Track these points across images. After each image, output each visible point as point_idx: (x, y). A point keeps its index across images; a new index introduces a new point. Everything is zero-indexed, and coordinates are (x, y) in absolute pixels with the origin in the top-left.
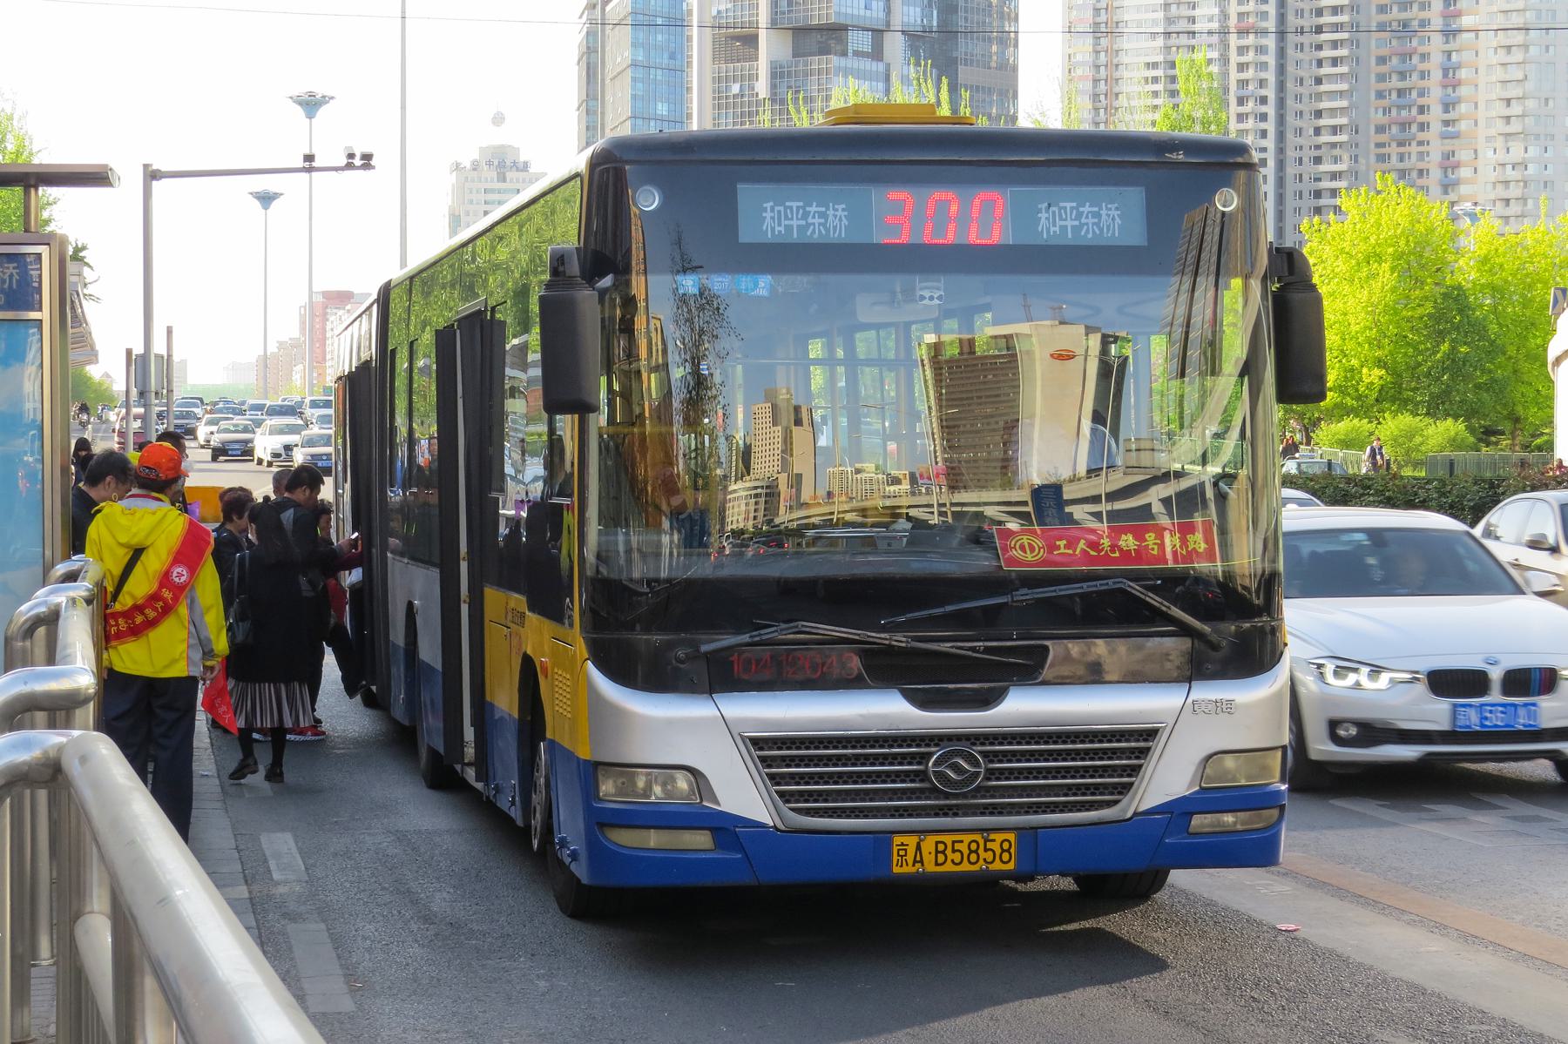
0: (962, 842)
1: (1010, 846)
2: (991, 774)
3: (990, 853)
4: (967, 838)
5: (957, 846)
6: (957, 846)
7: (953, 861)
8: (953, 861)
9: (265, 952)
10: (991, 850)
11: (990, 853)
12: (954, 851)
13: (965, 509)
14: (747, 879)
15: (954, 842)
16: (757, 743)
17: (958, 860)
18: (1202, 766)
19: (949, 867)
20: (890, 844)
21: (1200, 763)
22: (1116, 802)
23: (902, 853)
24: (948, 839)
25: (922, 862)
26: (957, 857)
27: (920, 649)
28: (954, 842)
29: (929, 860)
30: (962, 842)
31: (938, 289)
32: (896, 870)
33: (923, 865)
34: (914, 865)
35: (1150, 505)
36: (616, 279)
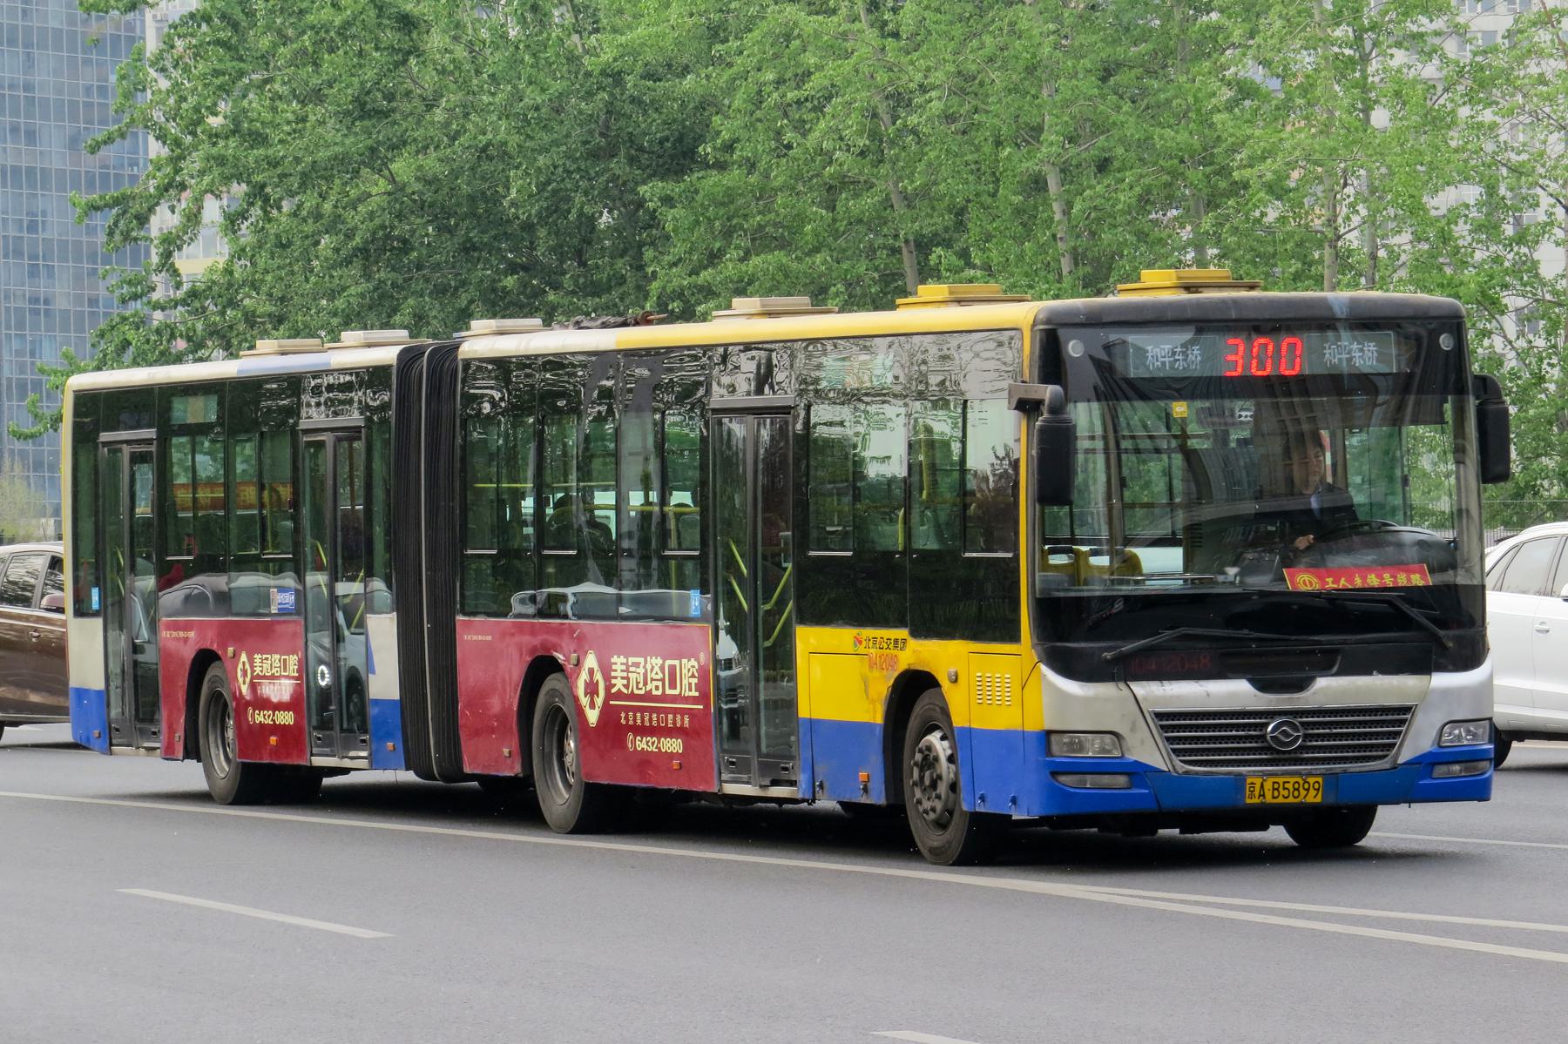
2: (1306, 737)
4: (1292, 780)
16: (1160, 716)
19: (1280, 800)
22: (1385, 756)
24: (1281, 780)
26: (1286, 793)
32: (1248, 801)
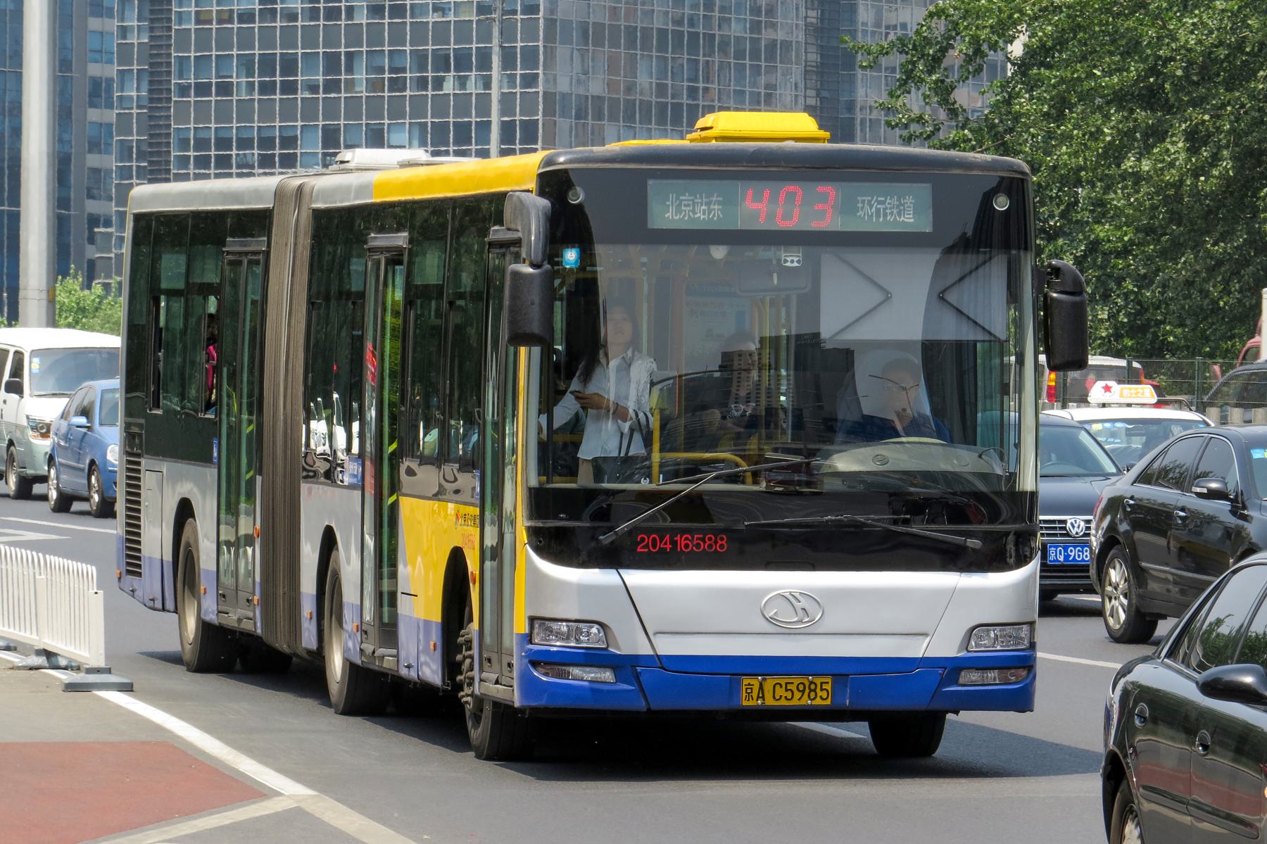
0: (792, 683)
1: (805, 688)
3: (825, 692)
5: (825, 686)
6: (825, 686)
7: (821, 697)
8: (821, 697)
9: (1081, 773)
10: (790, 690)
11: (825, 692)
12: (822, 690)
13: (387, 372)
14: (641, 705)
15: (822, 683)
17: (789, 696)
18: (967, 640)
20: (739, 683)
21: (968, 631)
23: (749, 691)
25: (763, 698)
27: (1200, 580)
28: (822, 683)
29: (768, 695)
30: (792, 683)
31: (799, 256)
32: (745, 703)
33: (764, 699)
34: (757, 700)
35: (976, 445)
36: (729, 254)
